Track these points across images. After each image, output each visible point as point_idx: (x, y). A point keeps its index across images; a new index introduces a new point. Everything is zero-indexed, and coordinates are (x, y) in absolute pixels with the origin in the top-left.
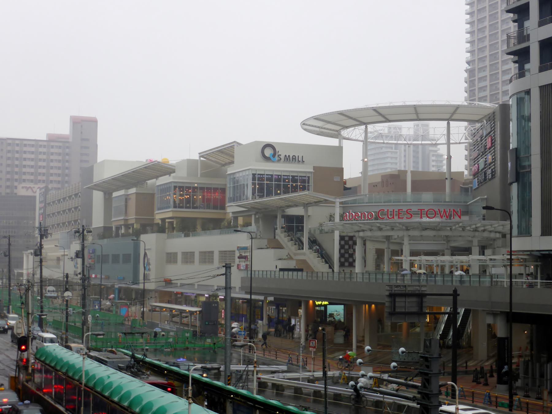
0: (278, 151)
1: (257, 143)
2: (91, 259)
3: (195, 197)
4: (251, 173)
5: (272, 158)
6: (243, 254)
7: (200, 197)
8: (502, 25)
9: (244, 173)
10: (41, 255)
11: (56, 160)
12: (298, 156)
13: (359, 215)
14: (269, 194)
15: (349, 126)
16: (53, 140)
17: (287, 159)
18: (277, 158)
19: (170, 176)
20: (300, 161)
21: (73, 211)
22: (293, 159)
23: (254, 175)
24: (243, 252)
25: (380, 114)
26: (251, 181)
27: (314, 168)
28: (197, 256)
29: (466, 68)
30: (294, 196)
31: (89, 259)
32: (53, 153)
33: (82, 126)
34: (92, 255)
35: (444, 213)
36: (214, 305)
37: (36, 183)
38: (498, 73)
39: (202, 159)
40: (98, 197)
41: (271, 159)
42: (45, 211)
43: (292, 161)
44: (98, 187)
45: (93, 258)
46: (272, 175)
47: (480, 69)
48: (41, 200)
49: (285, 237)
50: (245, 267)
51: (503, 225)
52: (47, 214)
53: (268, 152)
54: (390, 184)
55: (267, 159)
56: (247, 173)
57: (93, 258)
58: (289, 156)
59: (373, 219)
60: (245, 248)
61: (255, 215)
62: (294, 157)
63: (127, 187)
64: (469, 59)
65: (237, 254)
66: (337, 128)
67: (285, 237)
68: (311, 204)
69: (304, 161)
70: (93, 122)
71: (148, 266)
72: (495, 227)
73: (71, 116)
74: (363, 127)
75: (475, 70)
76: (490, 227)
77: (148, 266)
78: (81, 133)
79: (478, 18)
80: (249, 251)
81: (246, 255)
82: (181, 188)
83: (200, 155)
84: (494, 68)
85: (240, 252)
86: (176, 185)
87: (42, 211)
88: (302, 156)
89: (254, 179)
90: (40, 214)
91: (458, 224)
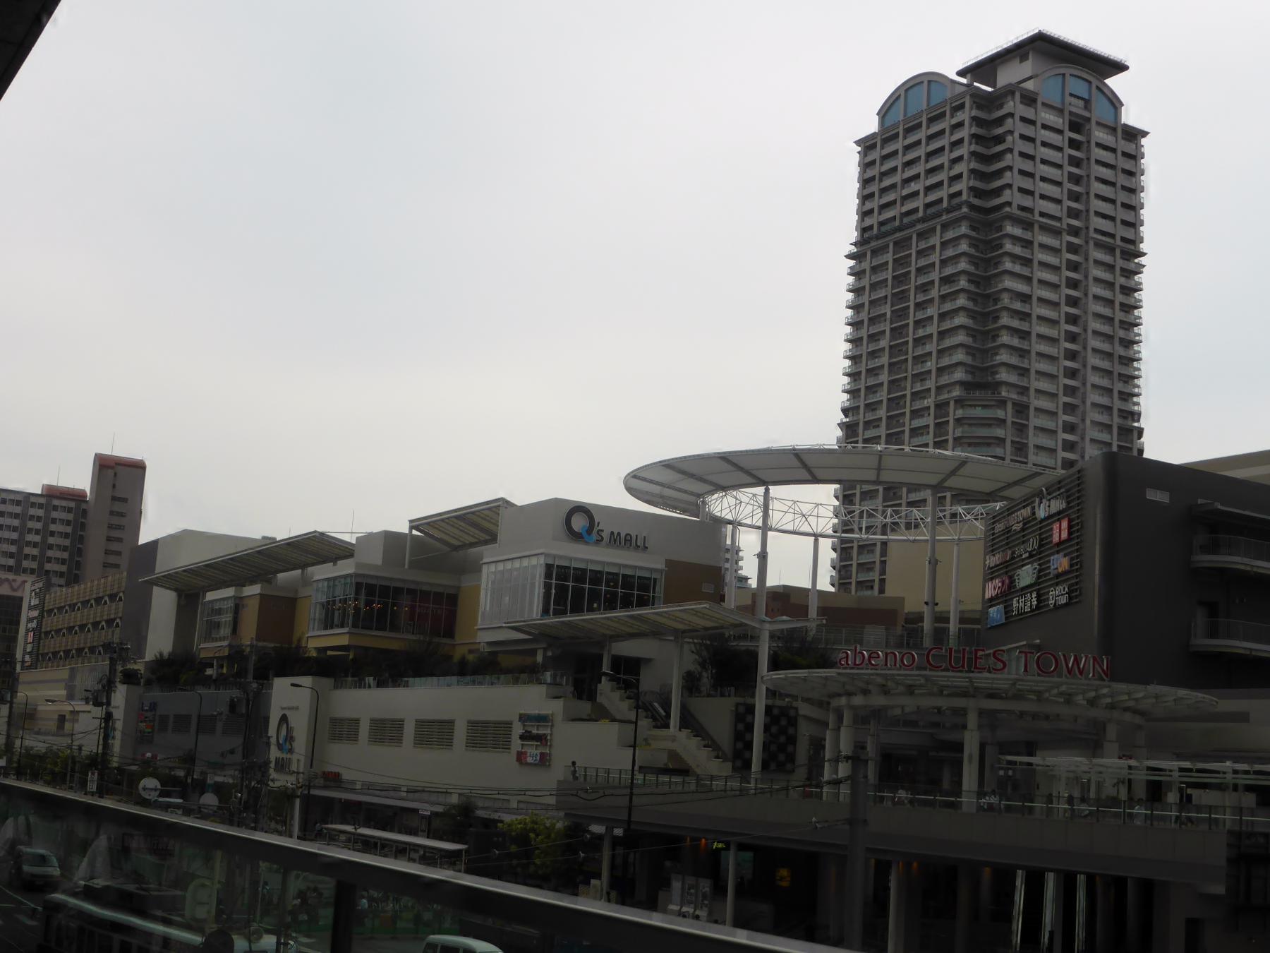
0: (599, 523)
1: (557, 502)
2: (145, 721)
3: (395, 608)
4: (542, 560)
5: (585, 534)
6: (535, 731)
7: (406, 609)
8: (914, 347)
9: (525, 562)
10: (108, 703)
11: (60, 533)
12: (637, 536)
13: (879, 657)
14: (577, 609)
15: (728, 487)
16: (54, 495)
17: (615, 541)
18: (594, 536)
19: (335, 564)
20: (639, 547)
21: (76, 631)
22: (625, 540)
23: (549, 568)
24: (532, 726)
25: (741, 469)
26: (542, 579)
27: (669, 563)
28: (409, 730)
29: (842, 420)
30: (665, 612)
31: (141, 722)
32: (56, 519)
33: (115, 474)
34: (149, 714)
35: (1075, 663)
36: (496, 839)
37: (17, 573)
38: (903, 432)
39: (415, 532)
40: (163, 603)
41: (583, 538)
42: (40, 624)
43: (625, 544)
44: (169, 581)
45: (150, 721)
46: (584, 571)
47: (868, 424)
48: (32, 604)
49: (622, 699)
50: (538, 758)
51: (1157, 697)
52: (43, 630)
53: (579, 523)
54: (772, 610)
55: (576, 536)
56: (534, 561)
57: (150, 721)
58: (619, 534)
59: (864, 665)
60: (542, 719)
61: (545, 650)
62: (628, 538)
63: (241, 583)
64: (847, 404)
65: (518, 729)
66: (697, 487)
67: (622, 699)
68: (697, 631)
69: (647, 548)
70: (136, 470)
71: (288, 744)
72: (1136, 700)
73: (96, 455)
74: (760, 490)
75: (858, 424)
76: (1126, 697)
77: (288, 744)
78: (114, 486)
79: (869, 333)
80: (550, 724)
81: (541, 732)
82: (371, 589)
83: (414, 524)
84: (894, 422)
85: (524, 726)
86: (360, 580)
87: (33, 625)
88: (645, 537)
89: (548, 575)
90: (27, 631)
91: (1058, 687)
